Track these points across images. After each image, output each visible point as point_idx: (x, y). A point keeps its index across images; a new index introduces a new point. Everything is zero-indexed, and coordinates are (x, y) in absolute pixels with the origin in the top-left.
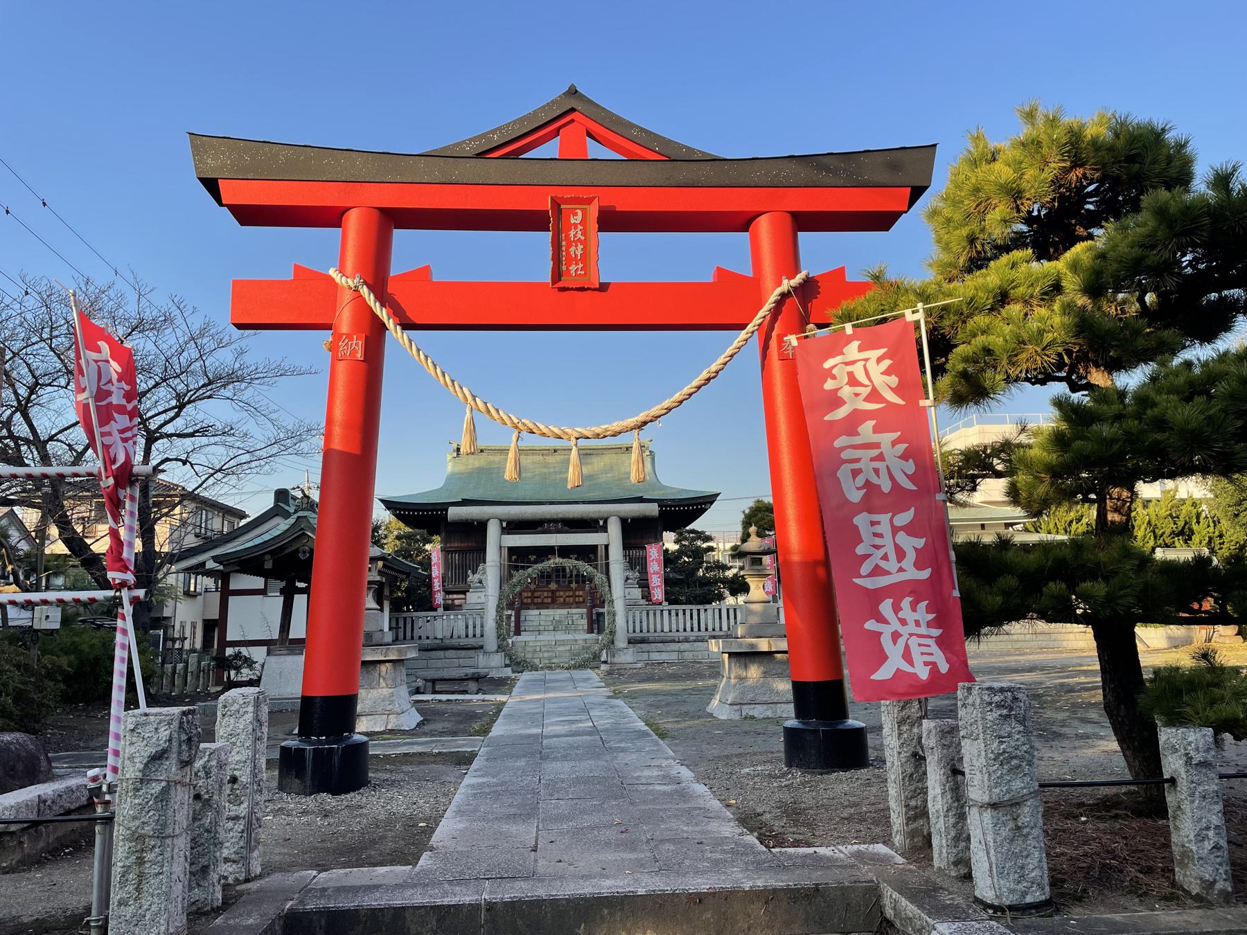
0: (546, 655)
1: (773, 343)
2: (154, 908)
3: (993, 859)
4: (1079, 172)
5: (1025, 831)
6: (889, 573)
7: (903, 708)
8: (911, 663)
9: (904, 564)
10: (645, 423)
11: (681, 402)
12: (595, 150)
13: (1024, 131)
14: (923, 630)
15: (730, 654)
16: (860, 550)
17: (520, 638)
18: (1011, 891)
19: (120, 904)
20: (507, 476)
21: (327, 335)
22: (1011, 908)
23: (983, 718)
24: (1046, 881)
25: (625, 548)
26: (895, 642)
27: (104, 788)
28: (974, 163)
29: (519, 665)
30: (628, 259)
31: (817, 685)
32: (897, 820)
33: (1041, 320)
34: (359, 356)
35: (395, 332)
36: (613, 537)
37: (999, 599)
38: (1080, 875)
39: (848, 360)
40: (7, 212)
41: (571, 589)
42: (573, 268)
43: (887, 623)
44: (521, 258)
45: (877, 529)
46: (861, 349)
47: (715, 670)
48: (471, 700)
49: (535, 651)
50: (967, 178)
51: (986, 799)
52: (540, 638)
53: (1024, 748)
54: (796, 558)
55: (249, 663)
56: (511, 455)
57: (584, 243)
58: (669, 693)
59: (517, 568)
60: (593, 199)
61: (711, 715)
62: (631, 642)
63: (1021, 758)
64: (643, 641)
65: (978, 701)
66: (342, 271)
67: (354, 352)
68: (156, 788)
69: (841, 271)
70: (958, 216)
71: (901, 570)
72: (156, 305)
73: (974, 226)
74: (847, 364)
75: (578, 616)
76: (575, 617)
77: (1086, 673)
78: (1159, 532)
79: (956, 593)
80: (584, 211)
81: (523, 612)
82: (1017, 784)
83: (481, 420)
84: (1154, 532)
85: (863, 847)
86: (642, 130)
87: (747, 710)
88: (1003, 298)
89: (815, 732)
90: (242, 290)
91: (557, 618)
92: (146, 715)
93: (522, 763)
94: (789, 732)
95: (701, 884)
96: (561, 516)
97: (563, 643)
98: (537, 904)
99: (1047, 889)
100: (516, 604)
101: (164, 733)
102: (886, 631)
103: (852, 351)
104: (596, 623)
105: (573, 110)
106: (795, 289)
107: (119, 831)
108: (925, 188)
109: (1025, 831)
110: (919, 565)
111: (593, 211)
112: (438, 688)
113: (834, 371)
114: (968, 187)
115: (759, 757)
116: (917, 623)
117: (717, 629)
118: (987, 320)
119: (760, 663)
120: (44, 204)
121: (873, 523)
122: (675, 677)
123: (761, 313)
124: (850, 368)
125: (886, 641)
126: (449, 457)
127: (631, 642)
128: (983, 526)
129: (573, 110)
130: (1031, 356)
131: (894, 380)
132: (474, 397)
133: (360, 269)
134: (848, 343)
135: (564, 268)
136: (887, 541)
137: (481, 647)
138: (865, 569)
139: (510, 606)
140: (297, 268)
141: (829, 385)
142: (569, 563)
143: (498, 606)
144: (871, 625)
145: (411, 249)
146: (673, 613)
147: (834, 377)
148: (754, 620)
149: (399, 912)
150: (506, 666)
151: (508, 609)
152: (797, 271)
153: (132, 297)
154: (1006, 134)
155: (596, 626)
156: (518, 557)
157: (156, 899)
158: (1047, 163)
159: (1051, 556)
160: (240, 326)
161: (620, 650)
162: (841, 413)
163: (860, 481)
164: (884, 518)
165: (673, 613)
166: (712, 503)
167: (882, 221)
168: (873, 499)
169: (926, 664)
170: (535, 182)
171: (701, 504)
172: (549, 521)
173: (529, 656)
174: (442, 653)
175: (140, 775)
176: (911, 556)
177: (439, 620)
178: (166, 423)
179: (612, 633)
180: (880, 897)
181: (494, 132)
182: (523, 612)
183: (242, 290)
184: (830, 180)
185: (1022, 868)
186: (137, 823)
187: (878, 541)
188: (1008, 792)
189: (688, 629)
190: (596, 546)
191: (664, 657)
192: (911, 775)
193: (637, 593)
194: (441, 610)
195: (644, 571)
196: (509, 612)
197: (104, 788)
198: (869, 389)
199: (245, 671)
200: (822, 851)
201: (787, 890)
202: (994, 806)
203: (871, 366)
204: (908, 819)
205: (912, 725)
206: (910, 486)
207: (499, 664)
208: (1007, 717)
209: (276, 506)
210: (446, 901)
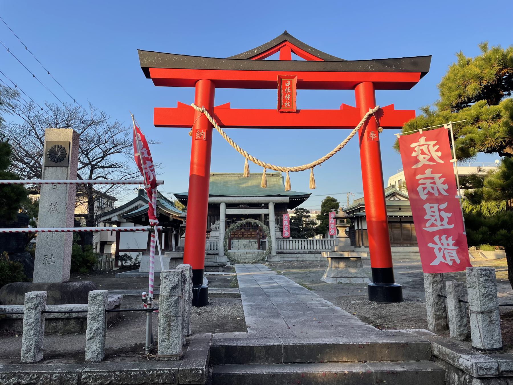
0: (243, 258)
1: (365, 134)
2: (175, 342)
3: (481, 332)
4: (506, 70)
5: (494, 322)
6: (437, 226)
7: (434, 277)
8: (445, 259)
9: (443, 223)
10: (315, 166)
11: (329, 157)
12: (294, 57)
13: (483, 55)
14: (451, 247)
15: (332, 258)
16: (426, 217)
17: (231, 251)
18: (489, 344)
19: (162, 341)
20: (262, 186)
21: (190, 130)
22: (488, 350)
23: (479, 280)
24: (501, 340)
25: (276, 215)
26: (440, 251)
27: (148, 299)
28: (463, 66)
29: (233, 261)
30: (308, 100)
31: (382, 269)
32: (431, 319)
33: (494, 128)
34: (204, 138)
35: (217, 130)
37: (481, 236)
38: (508, 339)
39: (421, 144)
40: (34, 76)
41: (250, 232)
42: (286, 104)
43: (437, 244)
44: (266, 100)
45: (433, 209)
46: (426, 140)
47: (323, 265)
48: (222, 275)
49: (238, 256)
50: (460, 72)
51: (479, 310)
52: (239, 251)
53: (494, 291)
54: (374, 219)
55: (130, 258)
56: (263, 177)
57: (291, 94)
58: (300, 273)
60: (295, 76)
61: (324, 282)
62: (278, 253)
63: (493, 295)
64: (282, 253)
65: (476, 274)
66: (196, 104)
67: (202, 136)
68: (174, 299)
69: (392, 106)
70: (454, 86)
71: (442, 225)
72: (97, 116)
73: (461, 90)
74: (420, 146)
76: (253, 243)
77: (504, 267)
78: (492, 212)
79: (465, 233)
80: (291, 81)
81: (232, 241)
82: (491, 305)
83: (251, 164)
84: (489, 211)
85: (417, 330)
86: (313, 49)
87: (339, 280)
88: (477, 119)
89: (382, 287)
90: (158, 112)
92: (169, 272)
93: (260, 297)
94: (370, 287)
95: (363, 341)
97: (250, 253)
98: (302, 346)
99: (501, 343)
100: (230, 237)
101: (176, 279)
102: (436, 248)
103: (422, 140)
104: (261, 245)
105: (286, 41)
106: (374, 113)
107: (161, 314)
108: (427, 73)
109: (494, 322)
110: (449, 223)
111: (295, 81)
112: (207, 270)
113: (415, 149)
114: (460, 74)
115: (356, 297)
116: (448, 245)
117: (312, 248)
118: (471, 128)
119: (345, 262)
120: (49, 73)
121: (431, 207)
122: (299, 267)
123: (361, 122)
124: (422, 148)
125: (436, 251)
127: (278, 253)
128: (400, 209)
129: (286, 41)
130: (491, 142)
131: (440, 154)
132: (248, 155)
133: (203, 104)
134: (420, 137)
135: (282, 104)
136: (437, 213)
137: (218, 254)
138: (428, 224)
140: (179, 104)
141: (414, 154)
142: (252, 221)
143: (224, 238)
144: (430, 245)
145: (222, 96)
146: (294, 242)
147: (415, 151)
148: (342, 244)
149: (252, 348)
150: (228, 262)
152: (375, 106)
153: (89, 112)
154: (475, 54)
155: (261, 247)
157: (175, 339)
158: (493, 67)
159: (501, 220)
160: (157, 126)
161: (273, 256)
162: (420, 165)
163: (426, 191)
164: (435, 206)
165: (294, 242)
166: (308, 197)
167: (408, 86)
168: (432, 198)
169: (451, 260)
170: (272, 70)
171: (304, 198)
172: (242, 204)
173: (236, 258)
175: (169, 294)
176: (446, 220)
178: (99, 162)
179: (270, 249)
180: (431, 347)
181: (255, 49)
182: (232, 241)
183: (158, 112)
184: (389, 69)
185: (492, 335)
186: (168, 311)
187: (433, 214)
188: (488, 307)
189: (300, 248)
190: (261, 214)
191: (290, 259)
192: (437, 303)
193: (279, 233)
195: (281, 225)
197: (148, 299)
198: (429, 157)
199: (128, 261)
200: (402, 331)
201: (396, 344)
202: (482, 313)
203: (431, 147)
204: (436, 319)
205: (438, 284)
206: (446, 194)
208: (488, 280)
209: (139, 196)
210: (269, 344)
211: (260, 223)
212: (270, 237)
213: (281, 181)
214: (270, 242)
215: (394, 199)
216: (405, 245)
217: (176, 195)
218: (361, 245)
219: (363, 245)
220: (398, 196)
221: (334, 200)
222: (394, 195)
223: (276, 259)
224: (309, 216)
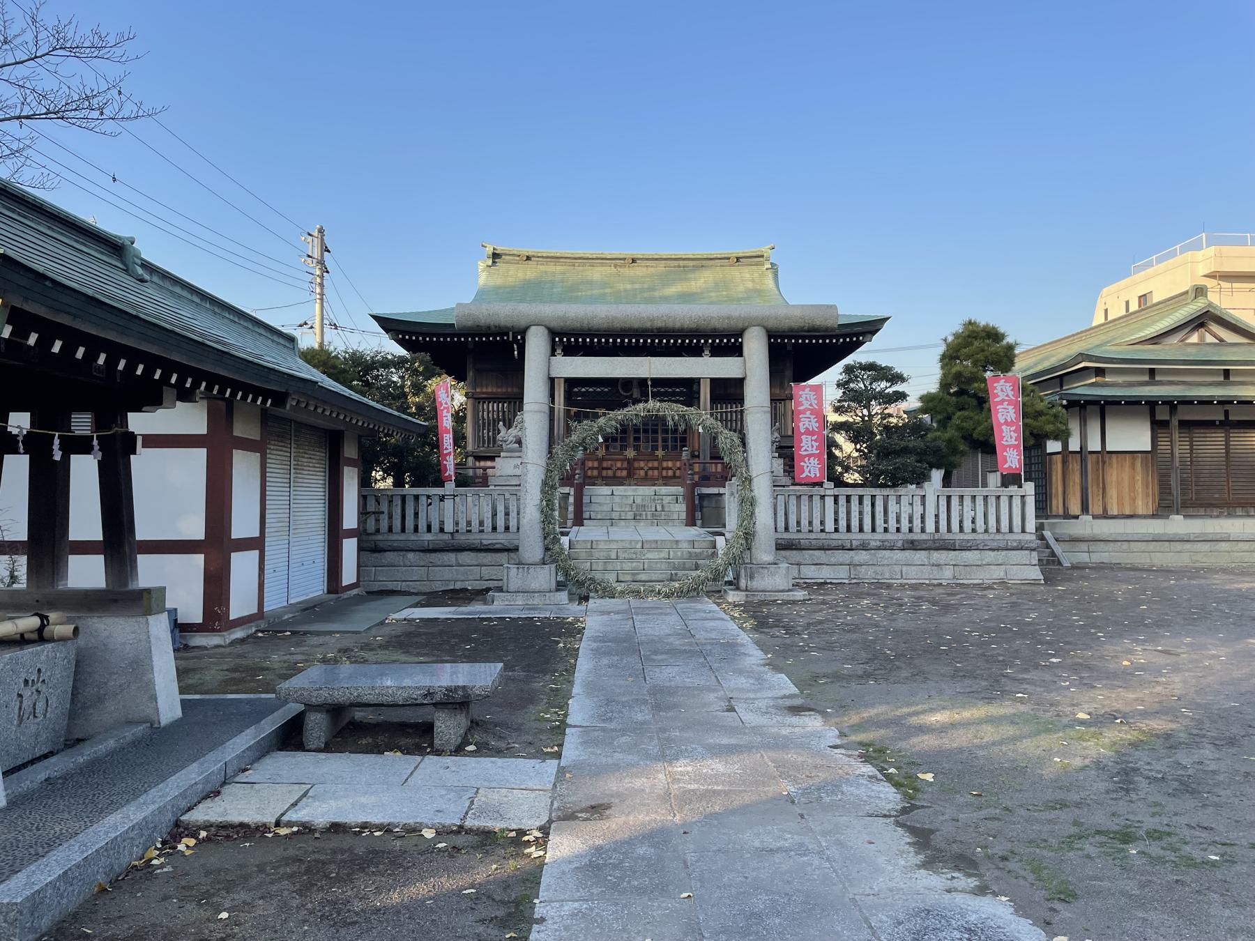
0: (627, 566)
36: (753, 366)
59: (579, 417)
62: (782, 546)
75: (671, 497)
76: (667, 500)
91: (639, 501)
96: (659, 324)
97: (656, 545)
100: (574, 479)
104: (702, 511)
126: (481, 265)
127: (782, 546)
128: (1227, 373)
139: (567, 480)
142: (672, 411)
143: (545, 483)
146: (842, 501)
151: (562, 485)
156: (583, 397)
161: (764, 566)
166: (874, 332)
171: (857, 335)
174: (450, 557)
177: (448, 503)
179: (748, 536)
191: (824, 574)
193: (779, 465)
194: (450, 487)
196: (566, 490)
207: (546, 586)
211: (702, 417)
212: (749, 480)
213: (770, 282)
214: (748, 503)
215: (1202, 338)
216: (1239, 511)
217: (389, 325)
218: (1075, 508)
219: (1085, 509)
220: (1215, 328)
221: (993, 335)
222: (1202, 325)
223: (775, 579)
224: (901, 396)
